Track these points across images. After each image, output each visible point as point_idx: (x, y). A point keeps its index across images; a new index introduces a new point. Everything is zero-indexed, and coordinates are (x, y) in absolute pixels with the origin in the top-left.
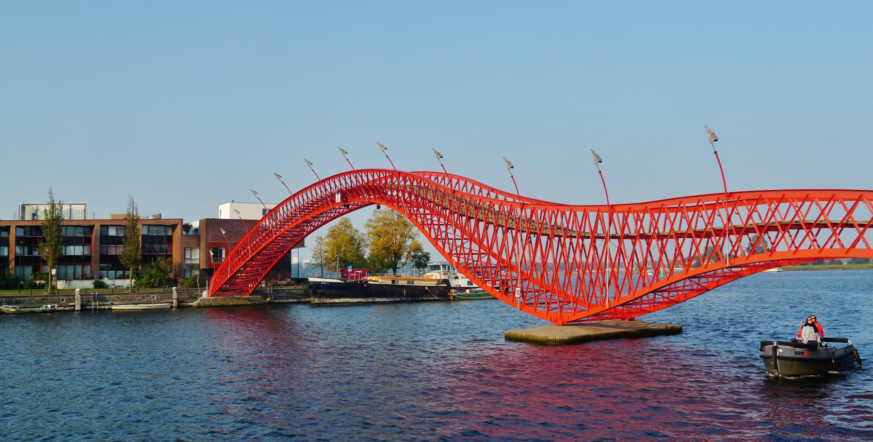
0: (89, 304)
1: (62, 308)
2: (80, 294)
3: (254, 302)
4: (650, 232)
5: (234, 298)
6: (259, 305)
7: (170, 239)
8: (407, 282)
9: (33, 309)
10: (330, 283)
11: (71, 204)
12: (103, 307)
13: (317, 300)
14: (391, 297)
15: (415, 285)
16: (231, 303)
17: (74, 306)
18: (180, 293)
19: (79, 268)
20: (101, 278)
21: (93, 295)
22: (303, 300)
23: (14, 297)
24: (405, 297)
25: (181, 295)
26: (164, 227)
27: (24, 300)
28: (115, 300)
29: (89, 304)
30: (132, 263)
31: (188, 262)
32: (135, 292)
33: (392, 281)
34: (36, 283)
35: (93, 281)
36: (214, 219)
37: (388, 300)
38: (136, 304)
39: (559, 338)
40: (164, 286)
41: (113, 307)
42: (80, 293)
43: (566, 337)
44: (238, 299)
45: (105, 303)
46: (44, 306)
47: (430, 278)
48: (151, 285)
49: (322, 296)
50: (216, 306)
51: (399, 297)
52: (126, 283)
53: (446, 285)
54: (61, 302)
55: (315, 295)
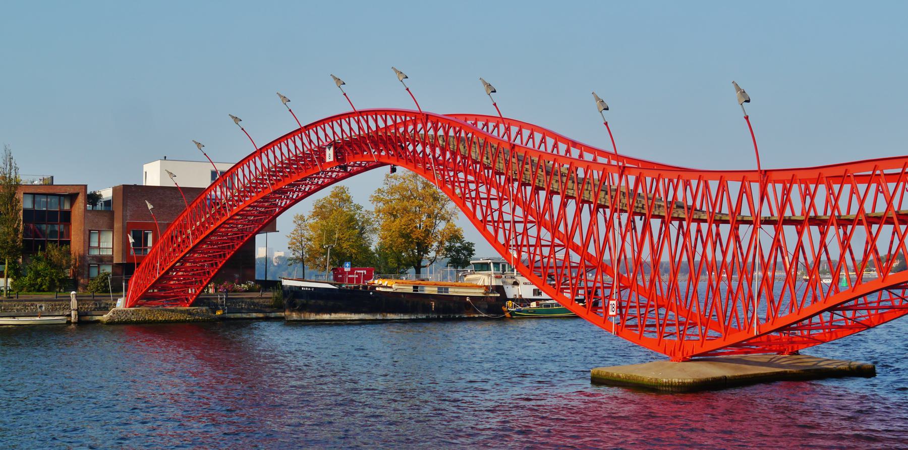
5: (166, 310)
8: (436, 289)
13: (295, 316)
14: (405, 312)
15: (426, 292)
18: (81, 300)
22: (273, 315)
24: (433, 312)
25: (83, 305)
26: (58, 197)
30: (9, 253)
31: (95, 252)
32: (12, 298)
33: (414, 287)
36: (135, 185)
37: (406, 317)
38: (14, 317)
43: (689, 380)
44: (173, 311)
47: (474, 283)
49: (303, 309)
50: (137, 323)
51: (423, 312)
53: (499, 295)
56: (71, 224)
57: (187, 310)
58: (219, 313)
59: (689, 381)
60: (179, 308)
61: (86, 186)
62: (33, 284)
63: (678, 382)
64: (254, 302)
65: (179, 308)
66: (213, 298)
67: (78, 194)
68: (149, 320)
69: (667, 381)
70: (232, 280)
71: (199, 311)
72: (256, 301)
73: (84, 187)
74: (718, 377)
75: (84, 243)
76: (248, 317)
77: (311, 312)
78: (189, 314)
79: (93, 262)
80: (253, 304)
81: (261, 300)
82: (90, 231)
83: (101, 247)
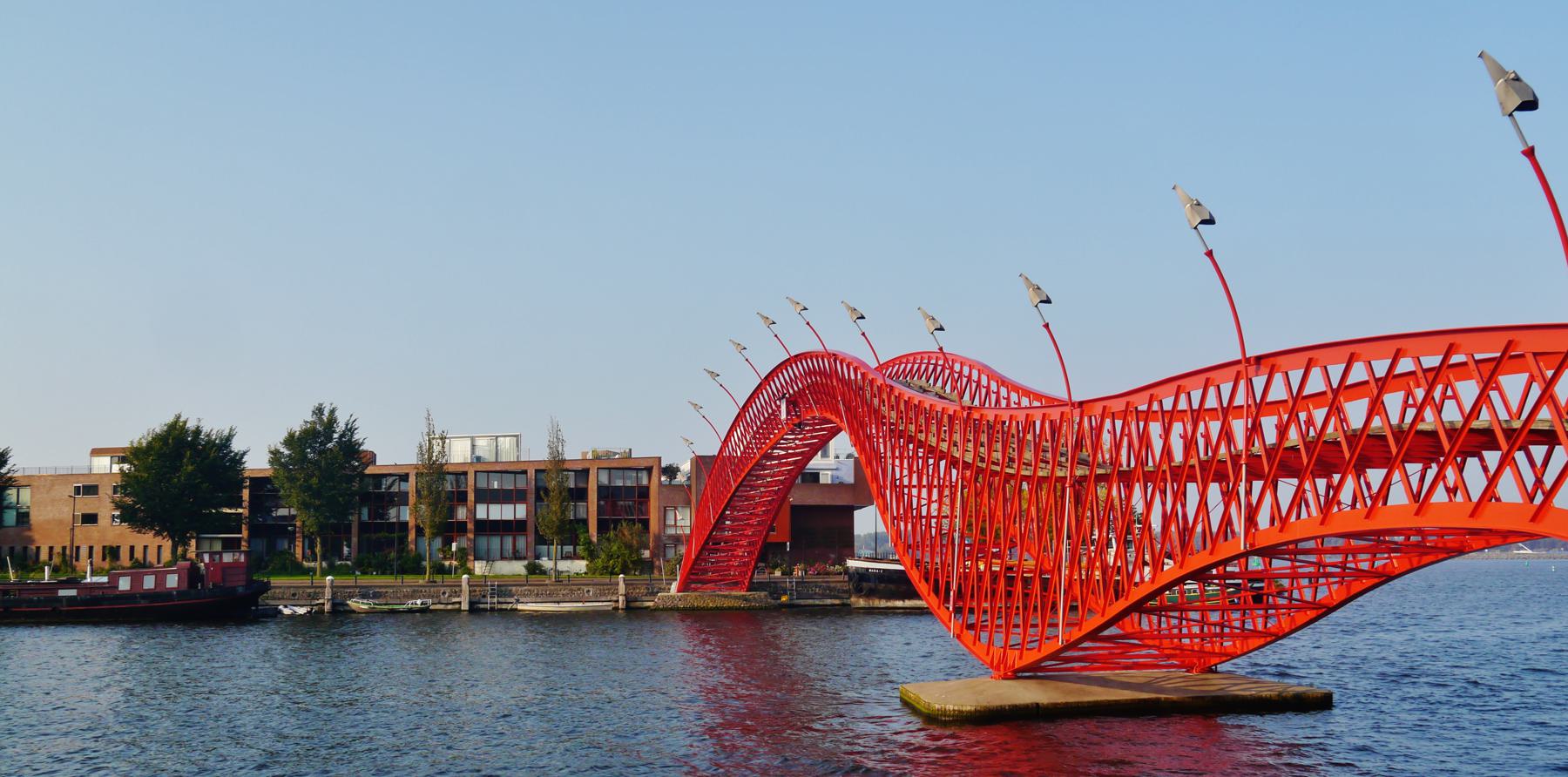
0: (483, 600)
2: (468, 583)
3: (753, 604)
4: (1129, 465)
5: (718, 596)
6: (762, 609)
7: (644, 493)
9: (395, 607)
12: (504, 606)
13: (862, 603)
17: (460, 603)
18: (632, 584)
19: (509, 541)
20: (538, 557)
23: (371, 586)
25: (634, 589)
26: (486, 474)
27: (387, 592)
28: (525, 596)
29: (483, 600)
30: (557, 534)
31: (671, 531)
32: (562, 581)
34: (443, 565)
35: (526, 562)
38: (558, 602)
39: (951, 708)
41: (520, 607)
42: (469, 582)
44: (726, 596)
45: (509, 600)
46: (410, 602)
48: (610, 570)
49: (871, 594)
54: (442, 596)
55: (859, 591)
59: (968, 708)
60: (734, 593)
61: (660, 458)
63: (954, 710)
65: (734, 593)
69: (940, 707)
70: (826, 559)
72: (832, 585)
73: (657, 460)
76: (821, 603)
77: (880, 598)
80: (829, 588)
81: (839, 585)
82: (665, 508)
83: (678, 524)
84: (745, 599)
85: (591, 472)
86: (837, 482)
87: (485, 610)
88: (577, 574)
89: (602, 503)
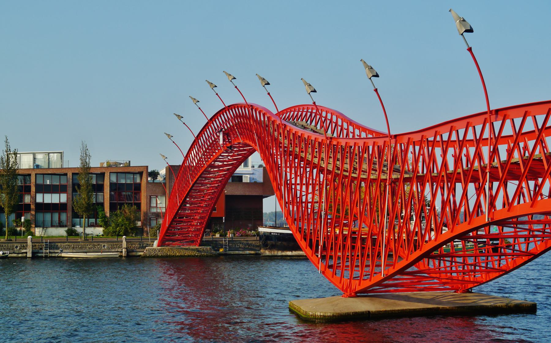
0: (41, 251)
1: (15, 255)
5: (182, 249)
7: (137, 187)
10: (280, 233)
11: (49, 153)
12: (53, 255)
13: (267, 253)
16: (178, 254)
17: (26, 253)
18: (130, 242)
19: (56, 216)
20: (74, 225)
21: (46, 242)
26: (59, 176)
28: (66, 248)
29: (41, 251)
31: (154, 210)
32: (88, 240)
35: (66, 229)
38: (86, 252)
40: (131, 235)
42: (32, 240)
44: (186, 249)
45: (56, 251)
50: (162, 257)
52: (99, 231)
54: (15, 249)
55: (265, 246)
56: (141, 192)
57: (197, 249)
58: (221, 251)
59: (329, 314)
60: (191, 247)
61: (147, 167)
62: (115, 231)
63: (320, 316)
64: (248, 243)
65: (191, 247)
66: (220, 241)
67: (143, 172)
68: (170, 255)
70: (246, 227)
71: (205, 249)
72: (250, 242)
73: (146, 167)
74: (361, 312)
75: (147, 204)
76: (243, 253)
78: (197, 251)
79: (153, 217)
80: (248, 244)
83: (158, 206)
84: (198, 250)
85: (106, 175)
86: (253, 181)
87: (42, 257)
88: (97, 236)
89: (113, 193)
